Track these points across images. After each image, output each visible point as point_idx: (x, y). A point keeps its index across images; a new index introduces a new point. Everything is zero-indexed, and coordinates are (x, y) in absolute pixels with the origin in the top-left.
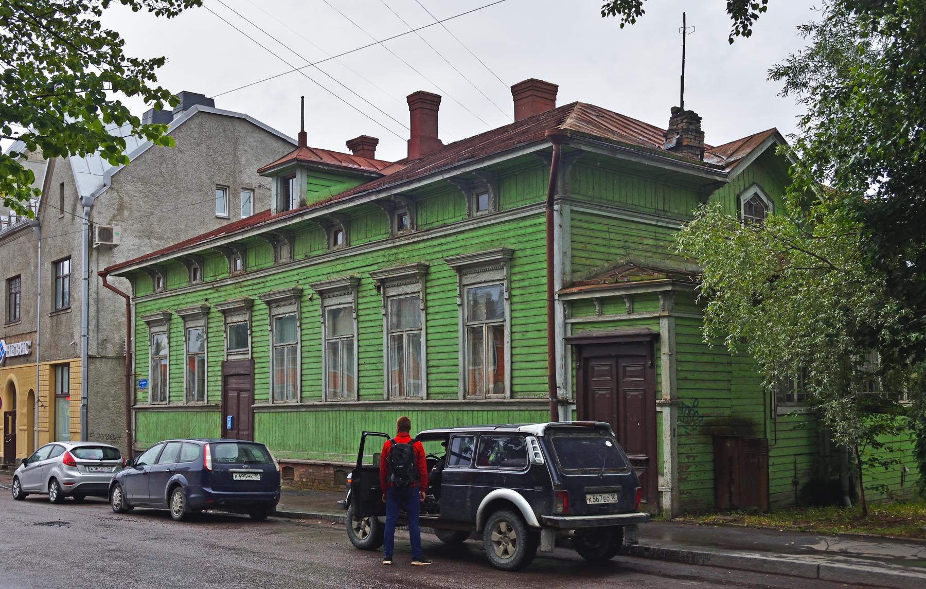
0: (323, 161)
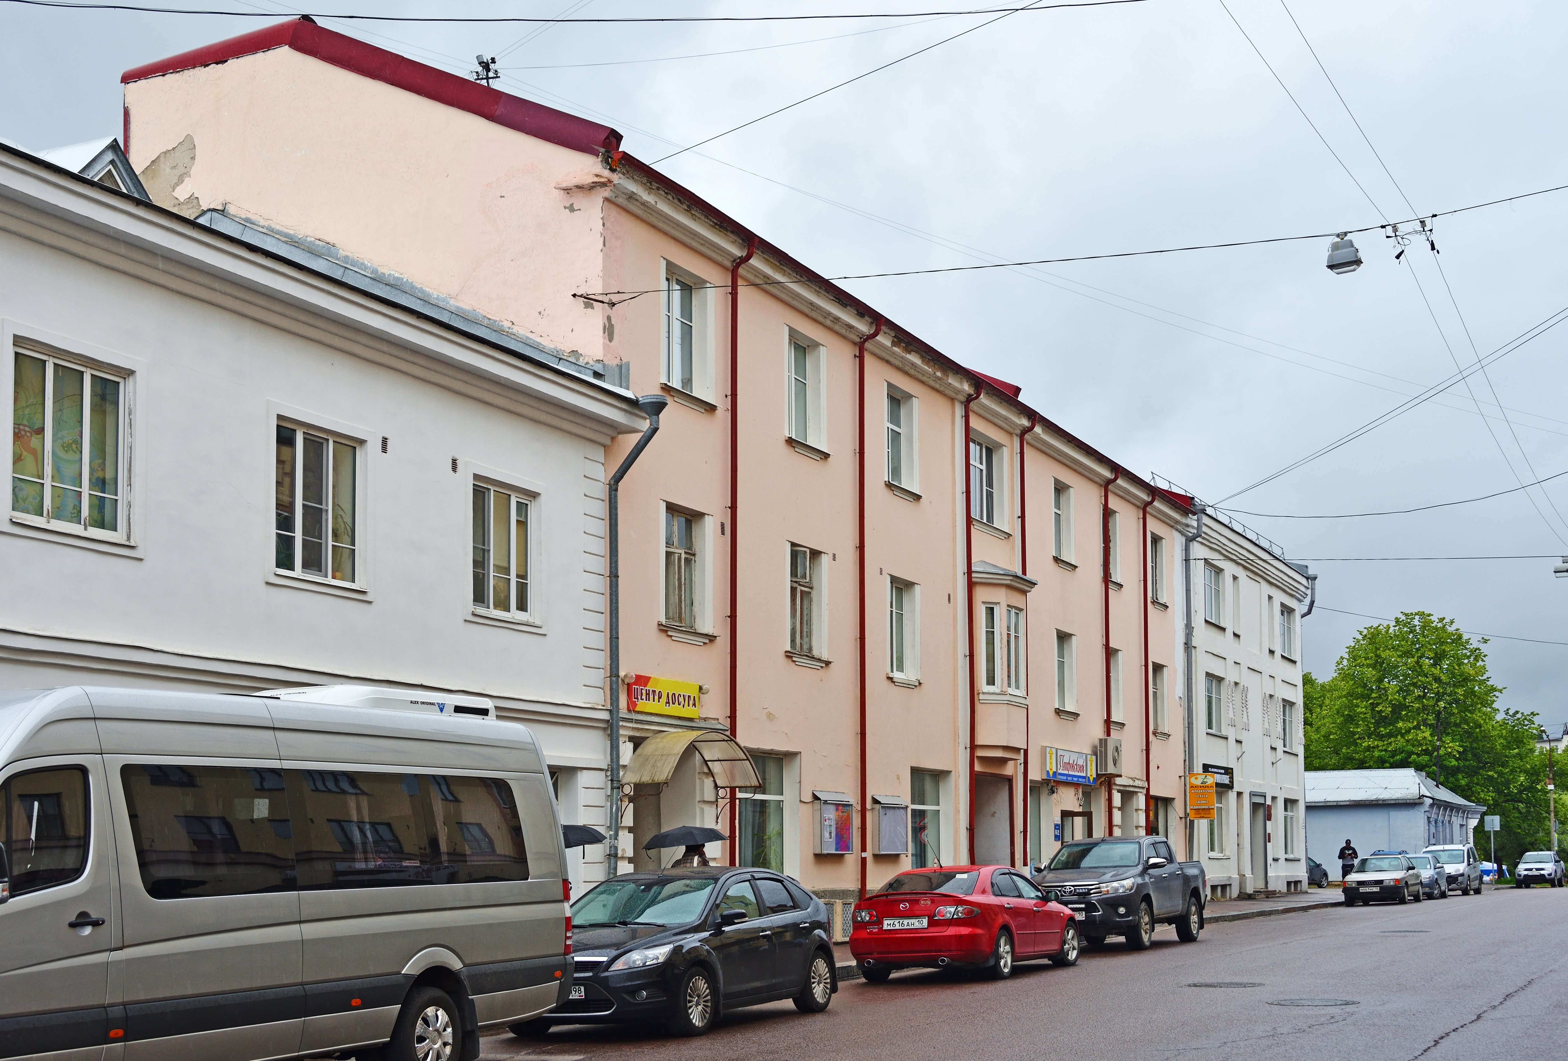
0: (1280, 597)
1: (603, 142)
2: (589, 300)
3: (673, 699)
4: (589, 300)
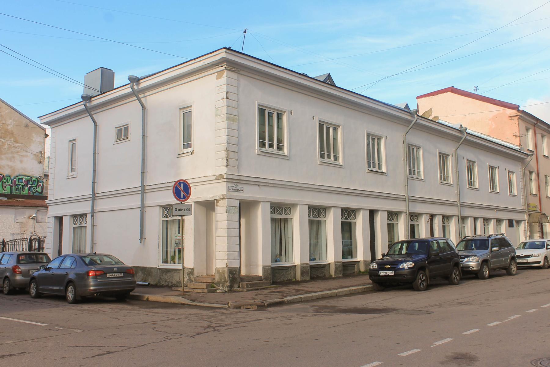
1: (516, 108)
2: (516, 136)
3: (533, 207)
4: (516, 136)
